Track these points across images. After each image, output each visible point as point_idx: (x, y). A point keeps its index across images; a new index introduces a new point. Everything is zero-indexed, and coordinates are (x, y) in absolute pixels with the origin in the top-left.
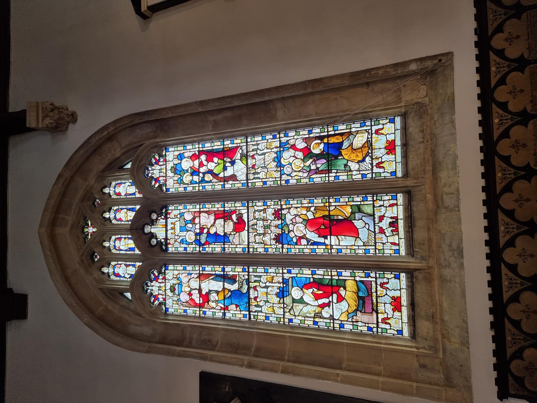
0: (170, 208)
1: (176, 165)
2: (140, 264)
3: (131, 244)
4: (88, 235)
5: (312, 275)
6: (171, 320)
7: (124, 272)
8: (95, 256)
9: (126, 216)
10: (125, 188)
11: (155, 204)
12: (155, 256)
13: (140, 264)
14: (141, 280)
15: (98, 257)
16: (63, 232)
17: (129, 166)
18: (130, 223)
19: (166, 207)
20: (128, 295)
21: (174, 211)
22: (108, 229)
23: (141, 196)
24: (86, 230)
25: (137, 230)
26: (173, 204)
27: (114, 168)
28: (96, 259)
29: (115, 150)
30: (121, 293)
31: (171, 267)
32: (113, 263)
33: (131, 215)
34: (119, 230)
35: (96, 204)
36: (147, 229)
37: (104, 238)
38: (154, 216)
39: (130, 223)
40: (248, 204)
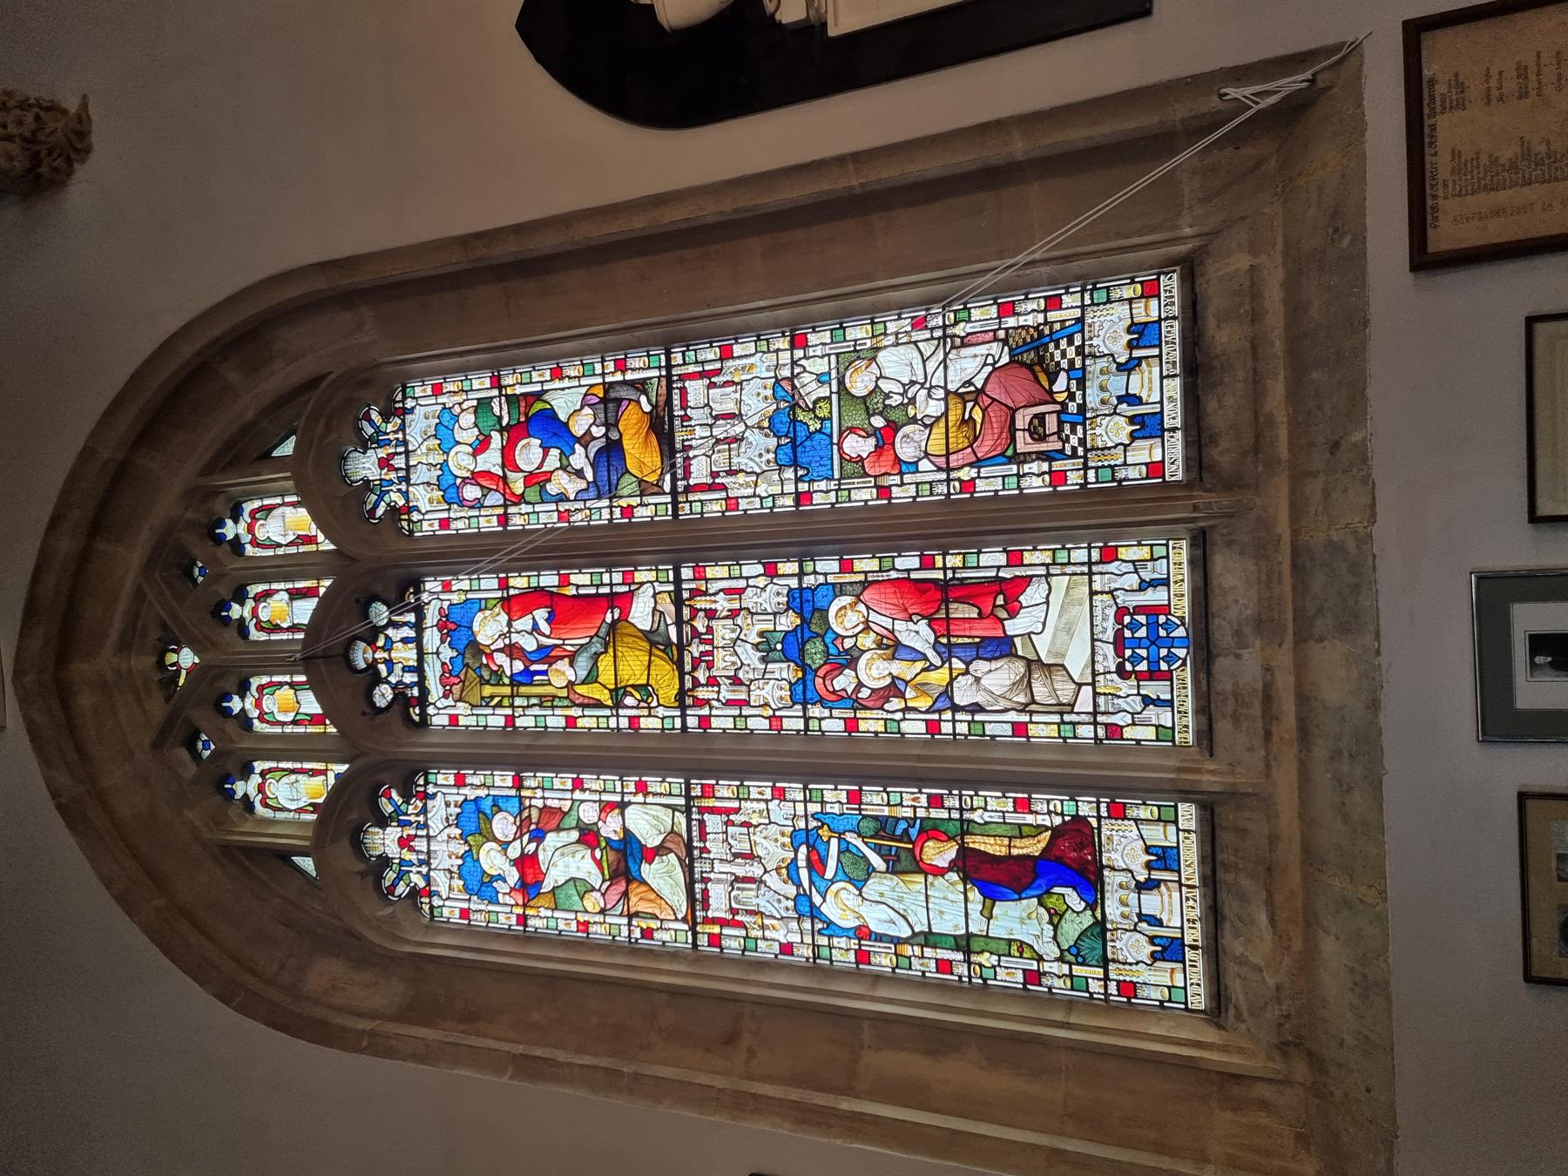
0: (428, 586)
1: (437, 448)
2: (343, 768)
3: (311, 704)
4: (178, 672)
5: (856, 719)
6: (443, 947)
7: (293, 793)
8: (204, 737)
9: (286, 611)
10: (285, 524)
11: (376, 567)
12: (383, 751)
13: (343, 768)
14: (348, 814)
15: (196, 571)
16: (98, 664)
17: (287, 448)
18: (301, 636)
19: (417, 585)
20: (307, 864)
21: (436, 595)
22: (235, 665)
23: (332, 547)
24: (171, 658)
25: (326, 656)
26: (435, 575)
27: (245, 454)
28: (207, 753)
29: (249, 397)
30: (284, 856)
31: (432, 585)
32: (259, 766)
33: (304, 611)
34: (271, 660)
35: (200, 581)
36: (361, 655)
37: (231, 767)
38: (380, 613)
39: (301, 636)
40: (668, 359)
